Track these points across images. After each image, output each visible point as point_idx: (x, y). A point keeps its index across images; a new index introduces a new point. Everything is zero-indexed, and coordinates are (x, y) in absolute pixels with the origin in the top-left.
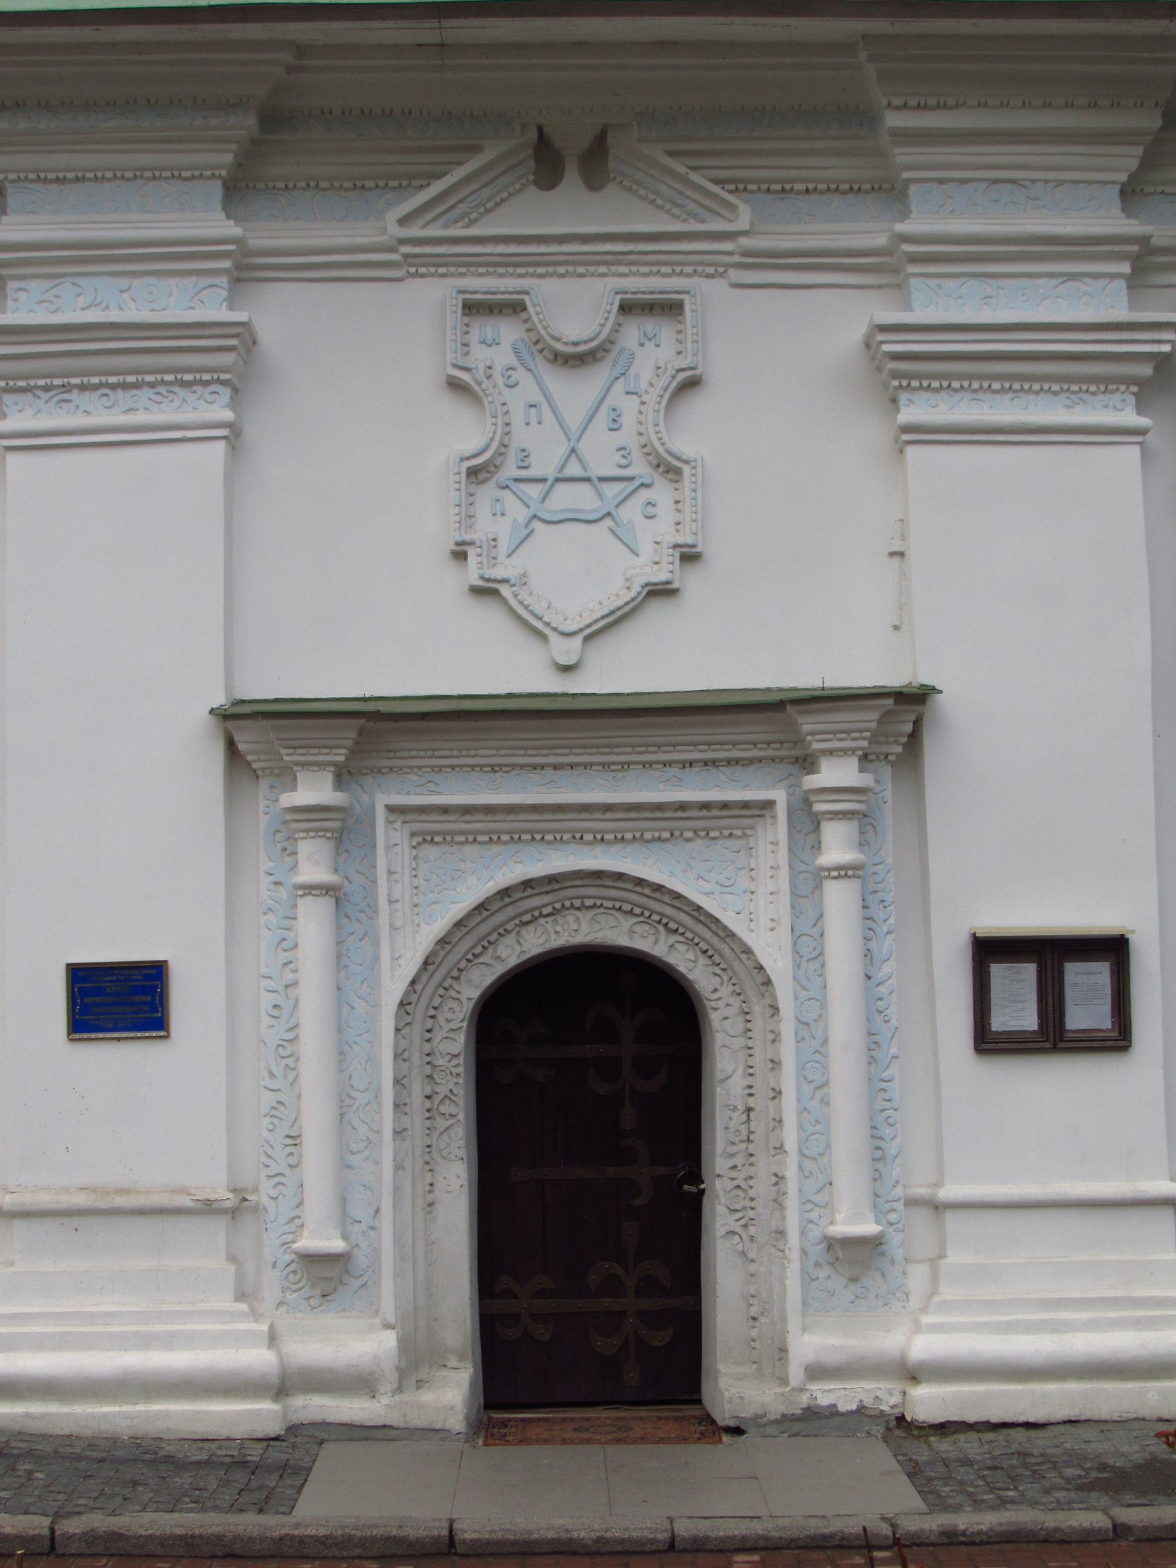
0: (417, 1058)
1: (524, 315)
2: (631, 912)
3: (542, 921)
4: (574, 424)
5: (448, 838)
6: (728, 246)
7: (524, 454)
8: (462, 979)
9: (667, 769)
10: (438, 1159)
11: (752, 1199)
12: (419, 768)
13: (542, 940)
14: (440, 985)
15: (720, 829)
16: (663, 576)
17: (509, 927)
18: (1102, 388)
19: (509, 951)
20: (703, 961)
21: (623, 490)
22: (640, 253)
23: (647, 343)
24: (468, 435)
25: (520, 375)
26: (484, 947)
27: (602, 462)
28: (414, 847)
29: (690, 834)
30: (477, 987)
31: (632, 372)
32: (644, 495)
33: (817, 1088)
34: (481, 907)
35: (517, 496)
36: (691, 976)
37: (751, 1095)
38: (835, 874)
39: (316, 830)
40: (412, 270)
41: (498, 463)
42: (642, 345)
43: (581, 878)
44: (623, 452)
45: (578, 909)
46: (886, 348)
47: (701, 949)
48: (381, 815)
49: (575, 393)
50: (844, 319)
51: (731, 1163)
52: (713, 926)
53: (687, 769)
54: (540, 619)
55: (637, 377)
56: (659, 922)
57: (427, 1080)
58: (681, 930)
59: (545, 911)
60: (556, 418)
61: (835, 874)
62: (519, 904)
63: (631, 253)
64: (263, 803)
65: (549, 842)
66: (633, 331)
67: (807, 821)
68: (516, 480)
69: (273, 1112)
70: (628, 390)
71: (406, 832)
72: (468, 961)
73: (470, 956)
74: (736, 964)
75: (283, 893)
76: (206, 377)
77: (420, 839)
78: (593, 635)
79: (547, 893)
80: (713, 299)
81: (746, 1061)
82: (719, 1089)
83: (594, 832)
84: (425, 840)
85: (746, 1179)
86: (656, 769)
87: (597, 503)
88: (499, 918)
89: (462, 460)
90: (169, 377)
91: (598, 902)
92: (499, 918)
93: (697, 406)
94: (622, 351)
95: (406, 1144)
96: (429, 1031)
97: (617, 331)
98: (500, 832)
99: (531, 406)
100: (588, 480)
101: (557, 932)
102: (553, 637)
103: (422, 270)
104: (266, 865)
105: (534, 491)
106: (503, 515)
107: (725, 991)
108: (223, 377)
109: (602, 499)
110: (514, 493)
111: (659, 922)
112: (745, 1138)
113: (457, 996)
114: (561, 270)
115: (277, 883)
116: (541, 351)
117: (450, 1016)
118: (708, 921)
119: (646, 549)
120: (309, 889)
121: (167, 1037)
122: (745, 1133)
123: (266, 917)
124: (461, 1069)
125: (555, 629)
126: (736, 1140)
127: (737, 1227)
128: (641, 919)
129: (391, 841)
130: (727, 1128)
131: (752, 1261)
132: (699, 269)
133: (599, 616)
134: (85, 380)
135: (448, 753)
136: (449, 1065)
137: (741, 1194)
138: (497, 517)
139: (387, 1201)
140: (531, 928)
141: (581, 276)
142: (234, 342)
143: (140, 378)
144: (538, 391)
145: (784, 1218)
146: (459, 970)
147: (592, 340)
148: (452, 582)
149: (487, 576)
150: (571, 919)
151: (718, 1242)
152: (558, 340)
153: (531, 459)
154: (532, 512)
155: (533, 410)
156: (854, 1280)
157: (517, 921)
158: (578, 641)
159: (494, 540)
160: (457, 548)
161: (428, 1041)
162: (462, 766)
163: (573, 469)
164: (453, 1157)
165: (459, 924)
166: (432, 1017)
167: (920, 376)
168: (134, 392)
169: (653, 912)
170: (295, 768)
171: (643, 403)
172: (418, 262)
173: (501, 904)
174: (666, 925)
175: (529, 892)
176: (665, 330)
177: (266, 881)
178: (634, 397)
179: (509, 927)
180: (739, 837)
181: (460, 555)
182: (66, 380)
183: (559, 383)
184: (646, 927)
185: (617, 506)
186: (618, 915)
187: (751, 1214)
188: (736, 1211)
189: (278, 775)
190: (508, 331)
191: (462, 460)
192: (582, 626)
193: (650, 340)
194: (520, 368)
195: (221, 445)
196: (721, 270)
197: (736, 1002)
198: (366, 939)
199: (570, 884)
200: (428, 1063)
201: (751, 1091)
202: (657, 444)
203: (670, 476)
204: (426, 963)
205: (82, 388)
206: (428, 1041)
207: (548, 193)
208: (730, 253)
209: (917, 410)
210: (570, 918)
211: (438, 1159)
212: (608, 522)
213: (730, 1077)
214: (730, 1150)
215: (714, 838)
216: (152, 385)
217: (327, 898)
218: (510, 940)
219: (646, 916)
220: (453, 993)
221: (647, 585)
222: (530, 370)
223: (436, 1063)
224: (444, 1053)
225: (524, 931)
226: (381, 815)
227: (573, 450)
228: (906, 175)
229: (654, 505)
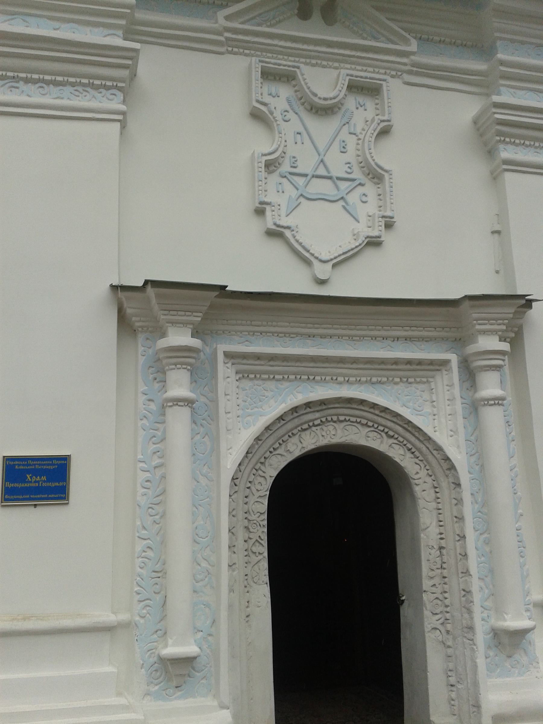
0: (241, 515)
1: (294, 83)
2: (366, 425)
3: (314, 428)
4: (321, 148)
5: (258, 376)
6: (405, 60)
7: (294, 159)
8: (267, 464)
9: (385, 341)
10: (252, 583)
11: (447, 606)
12: (241, 332)
13: (313, 441)
14: (254, 468)
15: (415, 377)
16: (375, 233)
17: (295, 431)
18: (186, 404)
19: (295, 447)
20: (409, 455)
21: (350, 185)
22: (358, 57)
23: (360, 108)
24: (261, 143)
25: (291, 115)
26: (280, 444)
27: (338, 171)
28: (237, 380)
29: (398, 380)
30: (275, 469)
31: (352, 122)
32: (360, 190)
33: (481, 534)
34: (281, 418)
35: (291, 183)
36: (402, 464)
37: (442, 539)
38: (492, 402)
39: (182, 364)
40: (230, 49)
41: (280, 162)
42: (357, 108)
43: (339, 403)
44: (348, 165)
45: (335, 422)
46: (497, 116)
47: (407, 447)
48: (221, 357)
49: (323, 129)
50: (463, 109)
51: (432, 582)
52: (417, 434)
53: (395, 342)
54: (308, 251)
55: (355, 125)
56: (383, 431)
57: (245, 529)
58: (396, 436)
59: (316, 422)
60: (312, 143)
61: (492, 402)
62: (302, 417)
63: (353, 56)
64: (141, 349)
65: (317, 382)
66: (351, 102)
67: (470, 374)
68: (291, 173)
69: (144, 554)
70: (351, 132)
71: (234, 371)
72: (271, 452)
73: (272, 450)
74: (430, 457)
75: (153, 406)
76: (109, 83)
77: (241, 375)
78: (339, 263)
79: (318, 411)
80: (395, 89)
81: (438, 517)
82: (422, 535)
83: (344, 376)
84: (243, 376)
85: (441, 593)
86: (378, 341)
87: (335, 192)
88: (290, 426)
89: (264, 155)
90: (85, 81)
91: (347, 418)
92: (290, 426)
93: (387, 143)
94: (346, 111)
95: (235, 573)
96: (246, 497)
97: (345, 99)
98: (289, 373)
99: (298, 133)
100: (330, 178)
101: (323, 436)
102: (316, 263)
103: (235, 50)
104: (143, 388)
105: (301, 181)
106: (283, 192)
107: (423, 473)
108: (120, 85)
109: (338, 190)
110: (289, 180)
111: (383, 431)
112: (440, 567)
113: (263, 474)
114: (314, 61)
115: (150, 400)
116: (303, 104)
117: (259, 487)
118: (413, 431)
119: (363, 219)
120: (177, 401)
121: (68, 503)
122: (439, 562)
123: (143, 422)
124: (265, 523)
125: (317, 258)
126: (434, 568)
127: (438, 625)
128: (372, 429)
129: (225, 371)
130: (428, 560)
131: (449, 647)
132: (388, 71)
133: (341, 253)
134: (29, 76)
135: (260, 323)
136: (258, 519)
137: (439, 602)
138: (279, 194)
139: (224, 614)
140: (308, 432)
141: (324, 67)
142: (130, 62)
143: (66, 79)
144: (302, 126)
145: (472, 618)
146: (265, 458)
147: (334, 98)
148: (255, 227)
149: (278, 222)
150: (331, 428)
151: (427, 635)
152: (316, 95)
153: (298, 163)
154: (300, 192)
155: (299, 136)
156: (510, 657)
157: (299, 428)
158: (329, 266)
159: (279, 205)
160: (260, 206)
161: (246, 503)
162: (266, 332)
163: (322, 171)
164: (261, 582)
165: (268, 428)
166: (248, 488)
167: (511, 136)
168: (61, 87)
169: (379, 425)
170: (167, 325)
171: (359, 139)
172: (234, 45)
173: (292, 417)
174: (387, 433)
175: (308, 410)
176: (370, 104)
177: (142, 399)
178: (354, 136)
179: (295, 431)
180: (424, 383)
181: (260, 212)
182: (16, 74)
183: (314, 124)
184: (376, 434)
185: (347, 194)
186: (359, 426)
187: (448, 616)
188: (436, 614)
189: (151, 332)
190: (285, 92)
191: (264, 155)
192: (332, 257)
193: (361, 106)
194: (291, 111)
195: (118, 124)
196: (399, 73)
197: (429, 480)
198: (207, 437)
199: (332, 406)
200: (246, 518)
201: (442, 536)
202: (368, 156)
203: (375, 180)
204: (247, 453)
205: (27, 81)
206: (246, 503)
207: (307, 21)
208: (405, 64)
209: (507, 153)
210: (330, 428)
211: (252, 583)
212: (341, 203)
213: (428, 527)
214: (431, 574)
215: (410, 383)
216: (73, 85)
217: (187, 407)
218: (295, 440)
219: (376, 427)
220: (260, 472)
221: (368, 237)
222: (296, 113)
223: (250, 518)
224: (255, 512)
225: (303, 434)
226: (221, 357)
227: (322, 161)
228: (497, 34)
229: (366, 196)
